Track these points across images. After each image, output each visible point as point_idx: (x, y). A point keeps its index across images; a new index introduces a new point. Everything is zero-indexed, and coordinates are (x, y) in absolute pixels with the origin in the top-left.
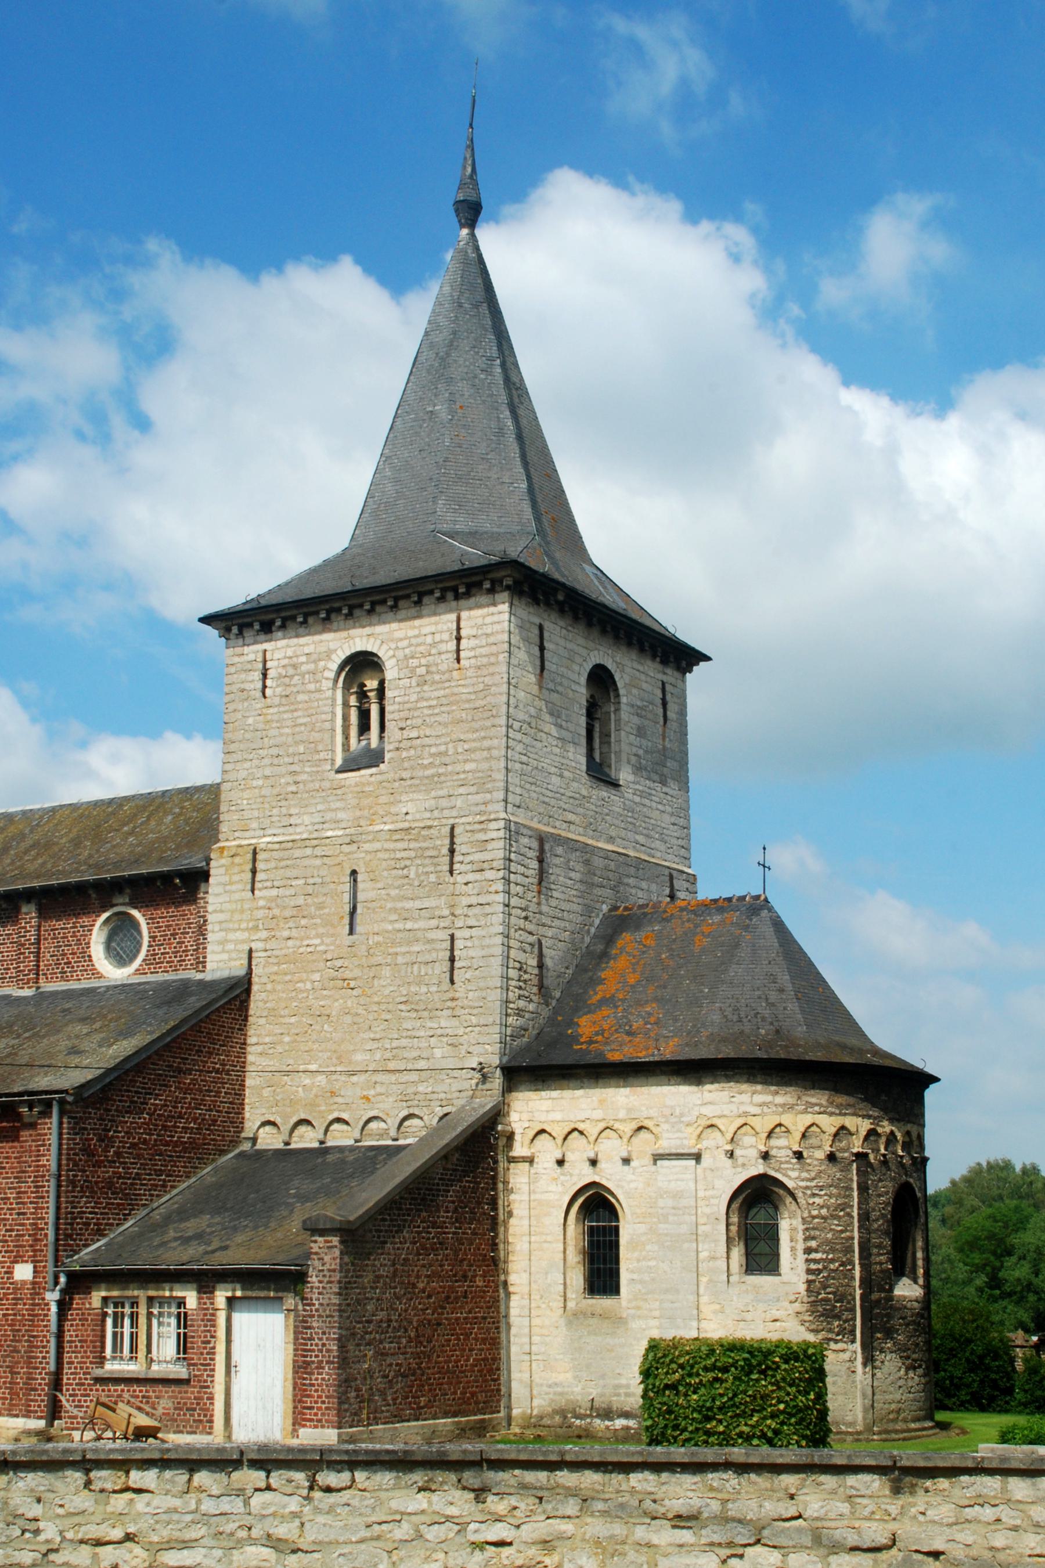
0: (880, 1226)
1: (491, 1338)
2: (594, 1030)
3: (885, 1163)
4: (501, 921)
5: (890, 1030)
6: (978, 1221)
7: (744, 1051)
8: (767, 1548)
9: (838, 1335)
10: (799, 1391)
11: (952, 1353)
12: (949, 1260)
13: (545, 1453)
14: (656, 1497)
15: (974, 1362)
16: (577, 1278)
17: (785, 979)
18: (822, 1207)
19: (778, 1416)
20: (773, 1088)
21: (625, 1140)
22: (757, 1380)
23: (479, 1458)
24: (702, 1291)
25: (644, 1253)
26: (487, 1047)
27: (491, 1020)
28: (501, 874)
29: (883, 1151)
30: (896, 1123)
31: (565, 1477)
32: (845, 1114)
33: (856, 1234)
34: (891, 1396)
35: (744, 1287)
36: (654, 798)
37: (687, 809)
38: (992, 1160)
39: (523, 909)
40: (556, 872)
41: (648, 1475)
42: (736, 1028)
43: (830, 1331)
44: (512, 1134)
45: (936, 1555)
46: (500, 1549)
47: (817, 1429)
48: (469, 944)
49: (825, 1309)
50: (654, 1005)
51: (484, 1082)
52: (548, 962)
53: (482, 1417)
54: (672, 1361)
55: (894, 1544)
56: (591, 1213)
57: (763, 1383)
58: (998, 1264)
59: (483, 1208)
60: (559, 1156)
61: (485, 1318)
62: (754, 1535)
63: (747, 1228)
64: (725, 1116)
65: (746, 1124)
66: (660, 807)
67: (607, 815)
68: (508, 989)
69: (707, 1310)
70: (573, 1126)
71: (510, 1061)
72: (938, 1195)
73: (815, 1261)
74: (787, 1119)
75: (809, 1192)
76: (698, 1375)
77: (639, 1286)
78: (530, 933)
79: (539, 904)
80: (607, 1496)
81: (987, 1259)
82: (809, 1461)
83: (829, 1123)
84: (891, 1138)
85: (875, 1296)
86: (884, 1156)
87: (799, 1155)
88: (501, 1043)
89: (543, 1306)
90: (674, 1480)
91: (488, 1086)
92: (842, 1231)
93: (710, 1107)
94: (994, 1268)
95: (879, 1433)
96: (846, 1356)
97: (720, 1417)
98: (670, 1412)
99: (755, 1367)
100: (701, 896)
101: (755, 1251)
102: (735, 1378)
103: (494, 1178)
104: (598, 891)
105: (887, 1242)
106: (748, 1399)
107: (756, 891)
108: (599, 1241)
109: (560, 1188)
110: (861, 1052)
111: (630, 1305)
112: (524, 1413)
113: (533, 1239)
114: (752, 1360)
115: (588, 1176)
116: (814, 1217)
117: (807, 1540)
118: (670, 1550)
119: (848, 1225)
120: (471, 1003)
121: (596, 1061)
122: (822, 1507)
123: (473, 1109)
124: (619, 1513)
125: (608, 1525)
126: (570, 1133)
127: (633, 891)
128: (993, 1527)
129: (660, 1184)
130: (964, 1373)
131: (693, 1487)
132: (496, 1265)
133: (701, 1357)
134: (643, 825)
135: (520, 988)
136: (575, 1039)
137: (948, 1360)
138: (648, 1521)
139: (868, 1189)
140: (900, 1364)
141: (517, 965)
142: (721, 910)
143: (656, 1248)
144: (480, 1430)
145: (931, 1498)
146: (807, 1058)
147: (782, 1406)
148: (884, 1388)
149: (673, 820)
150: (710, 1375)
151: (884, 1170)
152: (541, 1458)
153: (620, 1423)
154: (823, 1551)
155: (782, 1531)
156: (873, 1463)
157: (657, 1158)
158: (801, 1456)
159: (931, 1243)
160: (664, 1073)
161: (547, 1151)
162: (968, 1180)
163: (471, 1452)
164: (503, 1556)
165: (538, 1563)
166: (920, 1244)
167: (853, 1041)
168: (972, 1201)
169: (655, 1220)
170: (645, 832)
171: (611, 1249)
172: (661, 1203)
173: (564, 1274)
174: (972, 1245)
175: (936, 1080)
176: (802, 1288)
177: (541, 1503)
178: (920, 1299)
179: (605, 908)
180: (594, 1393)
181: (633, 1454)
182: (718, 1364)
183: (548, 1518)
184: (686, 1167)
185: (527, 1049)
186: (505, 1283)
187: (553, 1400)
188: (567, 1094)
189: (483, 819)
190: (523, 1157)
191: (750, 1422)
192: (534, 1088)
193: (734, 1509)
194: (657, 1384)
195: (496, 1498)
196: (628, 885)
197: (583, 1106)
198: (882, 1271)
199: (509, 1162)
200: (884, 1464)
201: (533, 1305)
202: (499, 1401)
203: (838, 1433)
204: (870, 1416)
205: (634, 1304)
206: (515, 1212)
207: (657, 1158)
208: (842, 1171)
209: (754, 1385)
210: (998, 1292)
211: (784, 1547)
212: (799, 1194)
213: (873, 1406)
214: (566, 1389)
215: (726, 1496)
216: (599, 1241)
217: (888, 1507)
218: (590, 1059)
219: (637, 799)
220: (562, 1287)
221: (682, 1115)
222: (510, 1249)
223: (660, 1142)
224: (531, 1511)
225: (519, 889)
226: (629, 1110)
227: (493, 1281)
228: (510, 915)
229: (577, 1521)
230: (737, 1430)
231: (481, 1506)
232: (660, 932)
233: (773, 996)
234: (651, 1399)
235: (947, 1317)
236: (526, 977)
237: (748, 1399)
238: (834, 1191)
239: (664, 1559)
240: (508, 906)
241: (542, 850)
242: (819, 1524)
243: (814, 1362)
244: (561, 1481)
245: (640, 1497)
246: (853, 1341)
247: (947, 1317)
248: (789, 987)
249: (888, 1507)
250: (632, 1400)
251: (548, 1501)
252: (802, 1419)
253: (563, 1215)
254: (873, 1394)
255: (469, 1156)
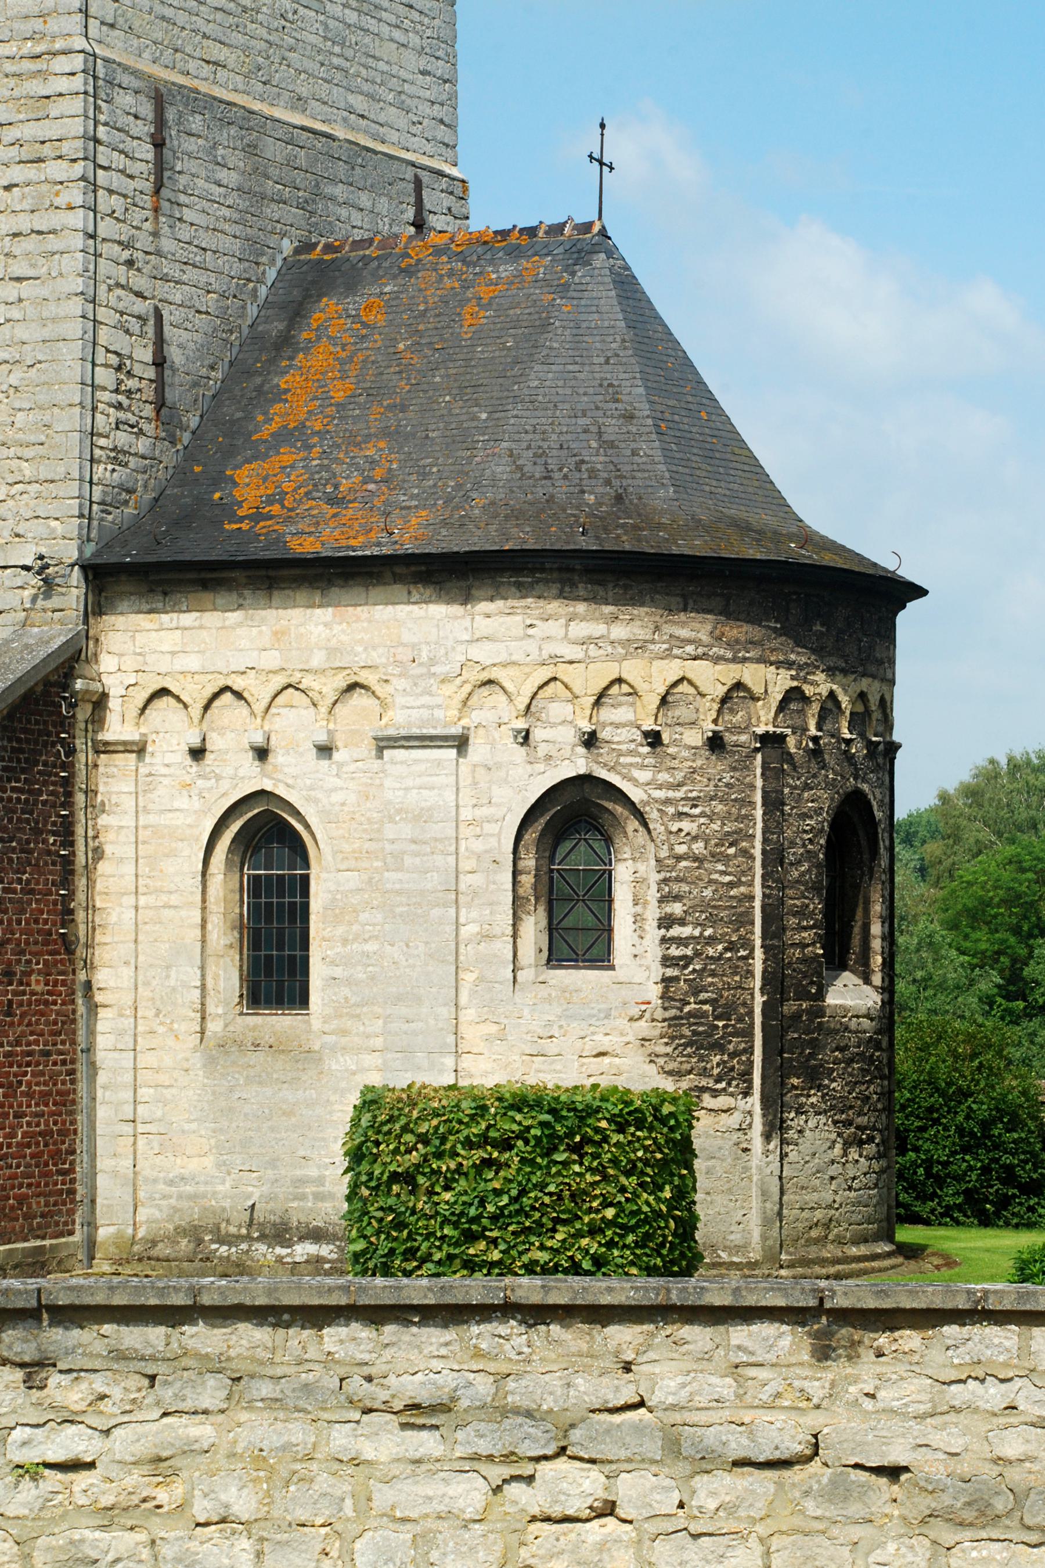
0: (802, 874)
1: (59, 1093)
2: (265, 494)
3: (816, 753)
4: (80, 268)
5: (837, 499)
6: (986, 869)
7: (554, 539)
8: (578, 1464)
9: (718, 1081)
10: (642, 1185)
11: (931, 1117)
12: (931, 944)
13: (162, 1292)
14: (373, 1371)
15: (972, 1134)
16: (227, 977)
17: (635, 394)
18: (695, 838)
19: (602, 1231)
20: (608, 609)
21: (323, 710)
22: (565, 1164)
23: (34, 1303)
24: (463, 999)
25: (355, 928)
26: (54, 524)
27: (61, 470)
28: (78, 169)
29: (813, 731)
30: (839, 677)
31: (201, 1337)
32: (744, 660)
33: (758, 891)
34: (815, 1196)
35: (543, 991)
36: (384, 15)
37: (451, 42)
38: (1018, 754)
39: (125, 245)
40: (190, 169)
41: (358, 1330)
42: (540, 491)
43: (704, 1073)
44: (104, 696)
45: (893, 1472)
46: (71, 1476)
47: (675, 1246)
48: (15, 313)
49: (695, 1033)
50: (382, 444)
51: (47, 595)
52: (175, 355)
53: (38, 1243)
54: (405, 1129)
55: (816, 1454)
56: (256, 850)
57: (577, 1168)
58: (1023, 952)
59: (45, 841)
60: (195, 741)
61: (47, 1054)
62: (555, 1439)
63: (551, 879)
64: (514, 663)
65: (555, 679)
66: (397, 34)
67: (291, 49)
68: (94, 409)
69: (472, 1034)
70: (221, 682)
71: (97, 554)
72: (913, 821)
73: (680, 941)
74: (633, 670)
75: (671, 810)
76: (455, 1154)
77: (346, 991)
78: (139, 294)
79: (155, 234)
80: (279, 1371)
81: (1003, 941)
82: (660, 1300)
83: (713, 677)
84: (830, 706)
85: (790, 1007)
86: (815, 739)
87: (654, 739)
88: (81, 516)
89: (161, 1029)
90: (406, 1338)
91: (55, 602)
92: (731, 885)
93: (487, 646)
94: (1014, 961)
95: (791, 1265)
96: (734, 1120)
97: (495, 1234)
98: (399, 1225)
99: (561, 1139)
100: (476, 224)
101: (568, 922)
102: (523, 1160)
103: (68, 783)
104: (272, 211)
105: (817, 905)
106: (547, 1200)
107: (586, 214)
108: (269, 905)
109: (196, 804)
110: (778, 538)
111: (327, 1028)
112: (120, 1235)
113: (142, 901)
114: (559, 1126)
115: (253, 779)
116: (679, 858)
117: (653, 1448)
118: (396, 1469)
119: (743, 873)
120: (20, 436)
121: (268, 555)
122: (684, 1385)
123: (27, 646)
124: (301, 1404)
125: (279, 1425)
126: (216, 696)
127: (344, 212)
128: (1002, 1420)
129: (389, 795)
130: (954, 1153)
131: (443, 1351)
132: (71, 952)
133: (460, 1122)
134: (364, 72)
135: (119, 406)
136: (227, 510)
137: (923, 1129)
138: (356, 1415)
139: (784, 804)
140: (834, 1136)
141: (114, 360)
142: (515, 253)
143: (379, 917)
144: (37, 1264)
145: (884, 1366)
146: (675, 550)
147: (610, 1213)
148: (803, 1181)
149: (423, 63)
150: (478, 1155)
151: (814, 767)
152: (153, 1301)
153: (303, 1250)
154: (683, 1468)
155: (608, 1431)
156: (781, 1302)
157: (384, 744)
158: (646, 1289)
159: (897, 912)
160: (398, 579)
161: (171, 731)
162: (972, 793)
163: (19, 1292)
164: (76, 1489)
165: (144, 1501)
166: (877, 908)
167: (763, 518)
168: (977, 832)
169: (378, 864)
170: (366, 87)
171: (292, 920)
172: (390, 831)
173: (203, 968)
174: (976, 915)
175: (919, 592)
176: (654, 992)
177: (152, 1386)
178: (874, 1013)
179: (287, 246)
180: (256, 1194)
181: (330, 1290)
182: (493, 1134)
183: (165, 1414)
184: (439, 763)
185: (135, 527)
186: (88, 985)
187: (176, 1210)
188: (212, 619)
189: (39, 49)
190: (124, 743)
191: (549, 1243)
192: (146, 607)
193: (517, 1393)
194: (377, 1173)
195: (65, 1379)
196: (332, 199)
197: (244, 643)
198: (803, 960)
199: (98, 752)
200: (802, 1304)
201: (140, 1028)
202: (71, 1212)
203: (714, 1265)
204: (775, 1233)
205: (334, 1024)
206: (108, 849)
207: (384, 744)
208: (734, 769)
209: (559, 1173)
210: (1021, 1004)
211: (611, 1462)
212: (652, 814)
213: (780, 1214)
214: (202, 1188)
215: (504, 1368)
216: (269, 905)
217: (806, 1384)
218: (258, 551)
219: (352, 17)
220: (197, 992)
221: (433, 661)
222: (98, 920)
223: (390, 713)
224: (134, 1401)
225: (116, 202)
226: (332, 652)
227: (64, 983)
228: (97, 255)
229: (221, 1418)
230: (525, 1259)
231: (35, 1394)
232: (396, 295)
233: (612, 428)
234: (365, 1201)
235: (924, 1048)
236: (131, 384)
237: (547, 1200)
238: (720, 808)
239: (385, 1487)
240: (93, 236)
241: (160, 122)
242: (677, 1417)
243: (672, 1129)
244: (191, 1344)
245: (342, 1371)
246: (747, 1093)
247: (924, 1048)
248: (644, 409)
249: (806, 1384)
250: (327, 1206)
251: (166, 1383)
252: (647, 1237)
253: (201, 855)
254: (782, 1193)
255: (19, 740)
